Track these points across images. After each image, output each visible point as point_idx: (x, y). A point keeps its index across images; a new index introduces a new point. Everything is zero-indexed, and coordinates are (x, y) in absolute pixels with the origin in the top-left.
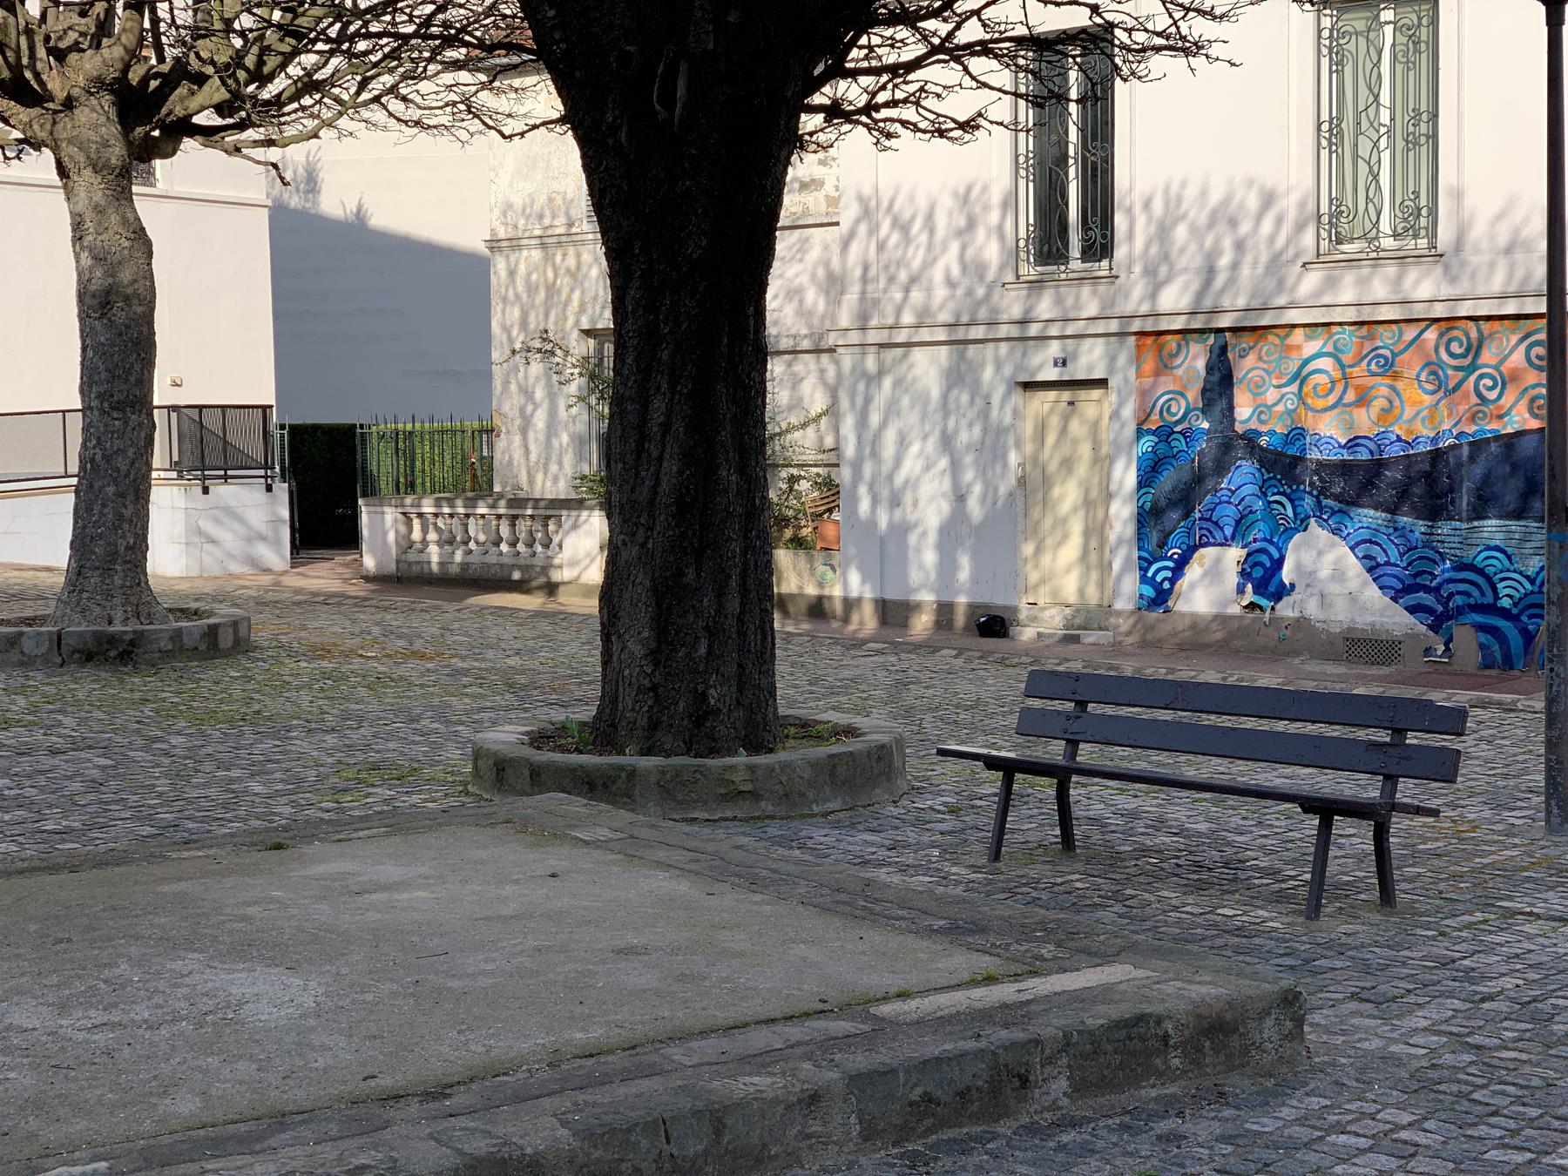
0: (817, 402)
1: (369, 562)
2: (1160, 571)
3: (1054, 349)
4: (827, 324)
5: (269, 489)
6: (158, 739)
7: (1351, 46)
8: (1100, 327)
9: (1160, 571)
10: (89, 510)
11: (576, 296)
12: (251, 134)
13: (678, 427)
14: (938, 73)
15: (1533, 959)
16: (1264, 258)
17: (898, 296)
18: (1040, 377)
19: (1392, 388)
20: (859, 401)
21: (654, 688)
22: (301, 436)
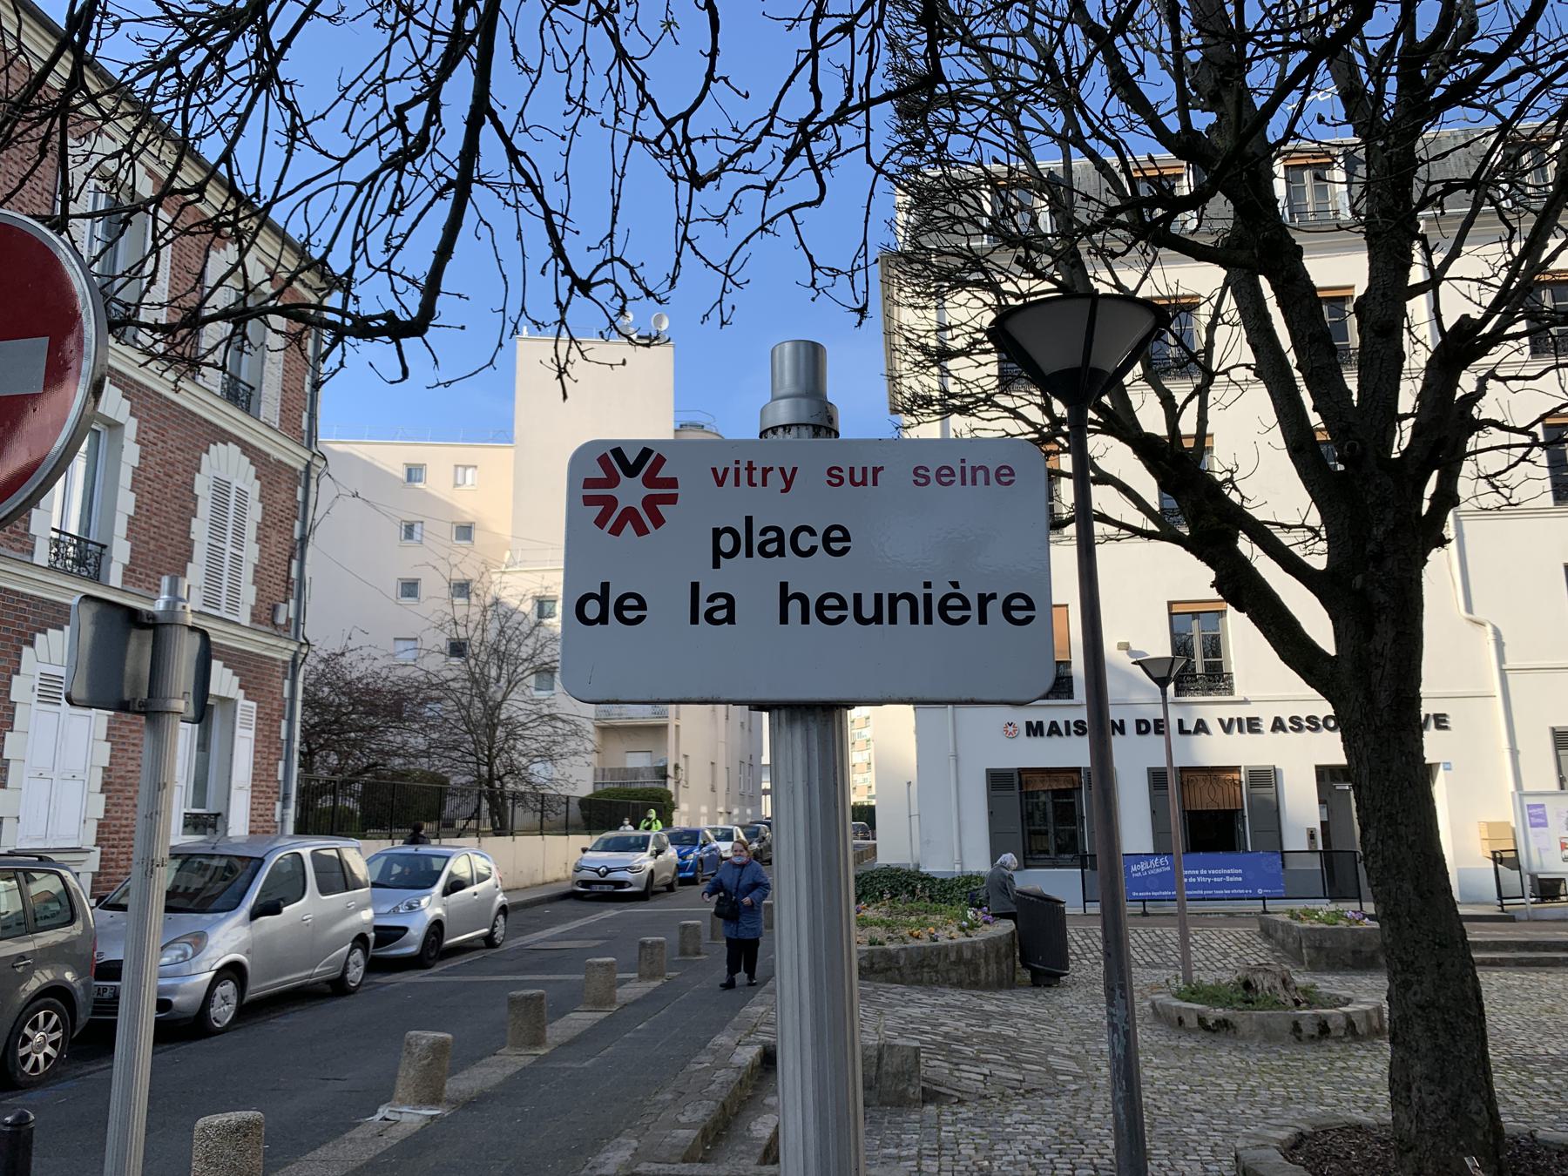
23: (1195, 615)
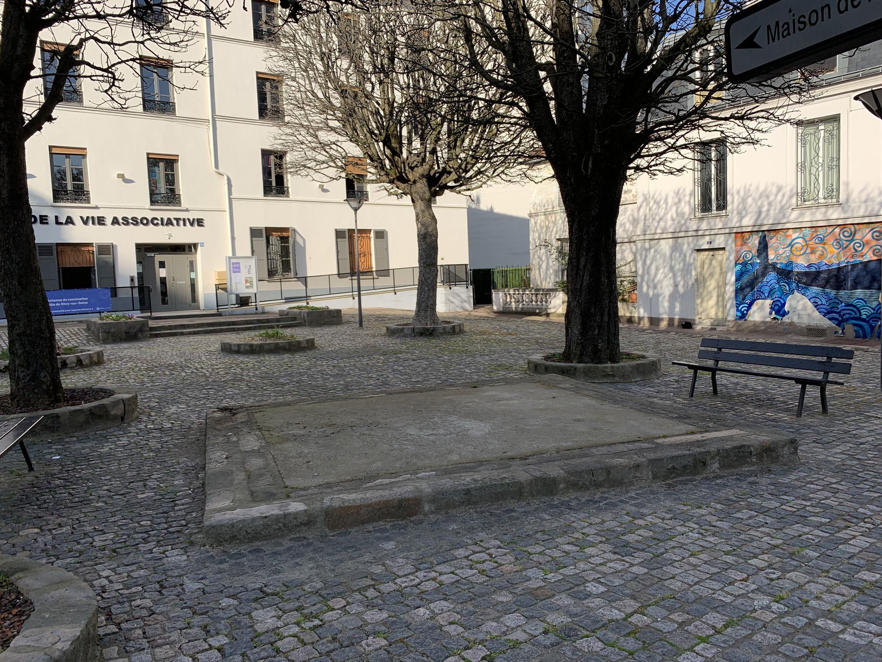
0: (630, 258)
1: (495, 308)
2: (743, 308)
3: (707, 239)
4: (633, 234)
5: (467, 287)
6: (440, 357)
7: (809, 138)
8: (723, 231)
9: (743, 308)
10: (421, 294)
11: (555, 229)
12: (463, 187)
13: (589, 266)
14: (670, 155)
15: (878, 431)
16: (778, 207)
17: (656, 224)
18: (702, 248)
19: (823, 248)
20: (643, 257)
21: (582, 343)
22: (476, 272)
23: (68, 156)
